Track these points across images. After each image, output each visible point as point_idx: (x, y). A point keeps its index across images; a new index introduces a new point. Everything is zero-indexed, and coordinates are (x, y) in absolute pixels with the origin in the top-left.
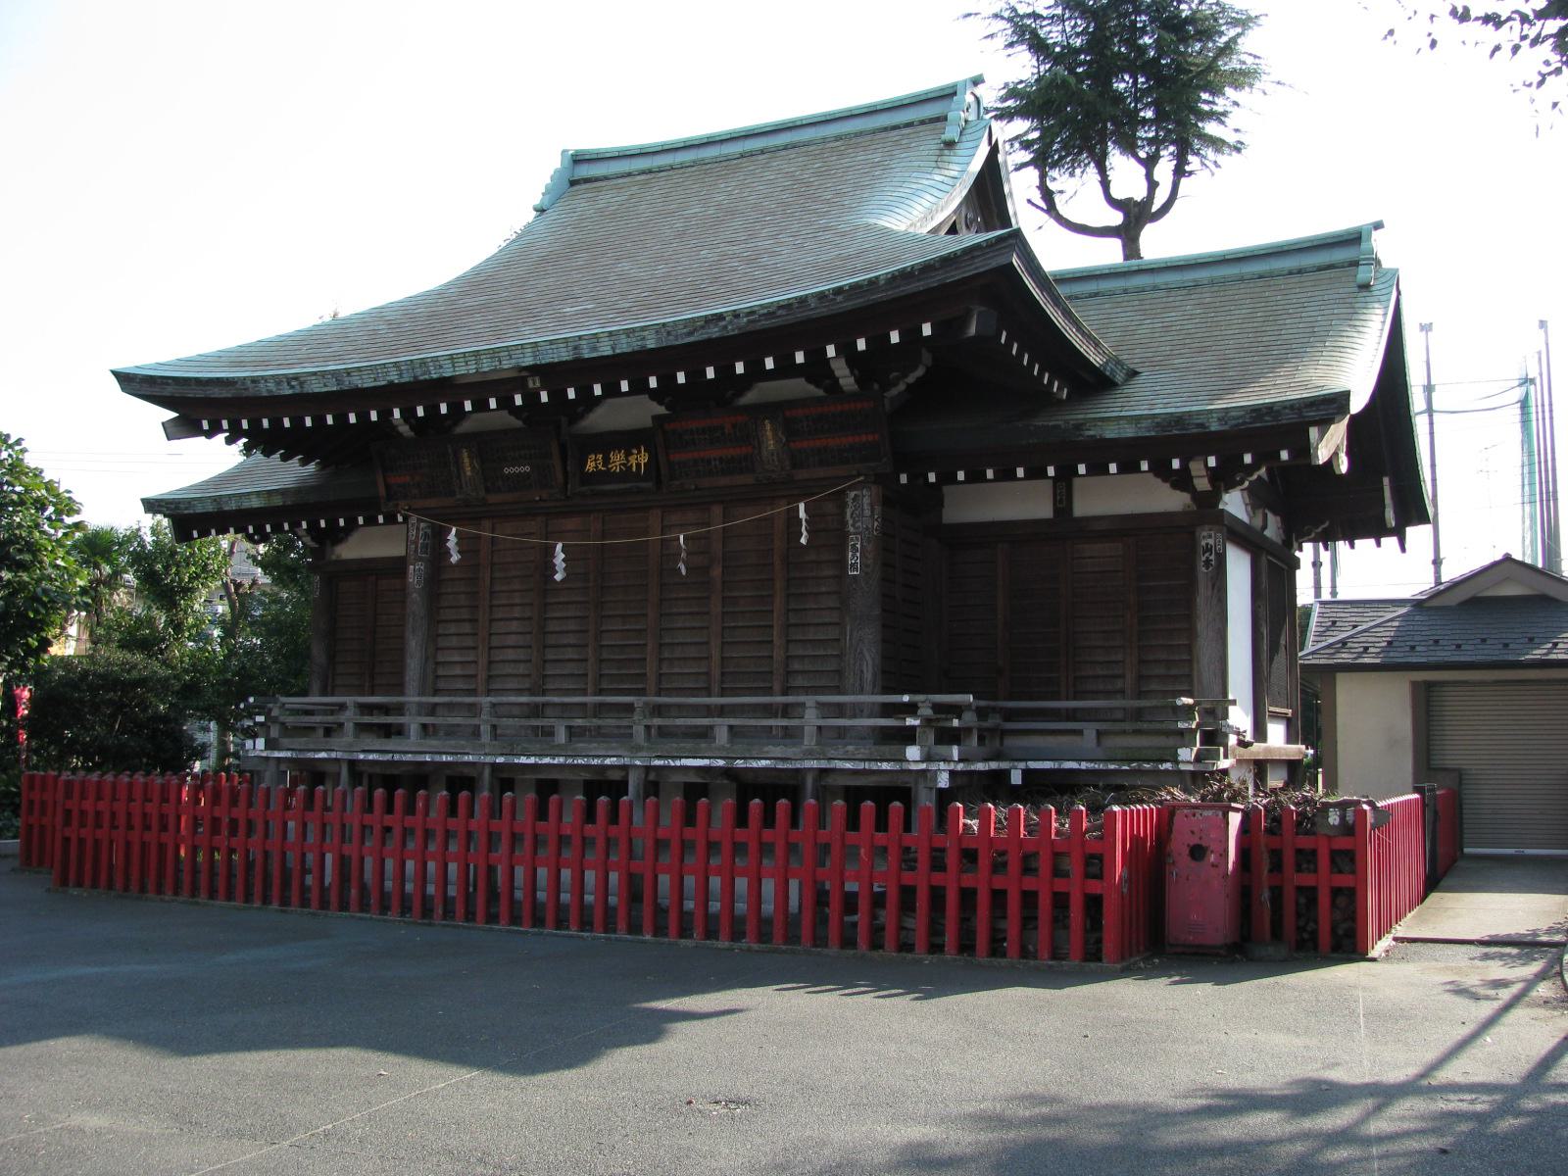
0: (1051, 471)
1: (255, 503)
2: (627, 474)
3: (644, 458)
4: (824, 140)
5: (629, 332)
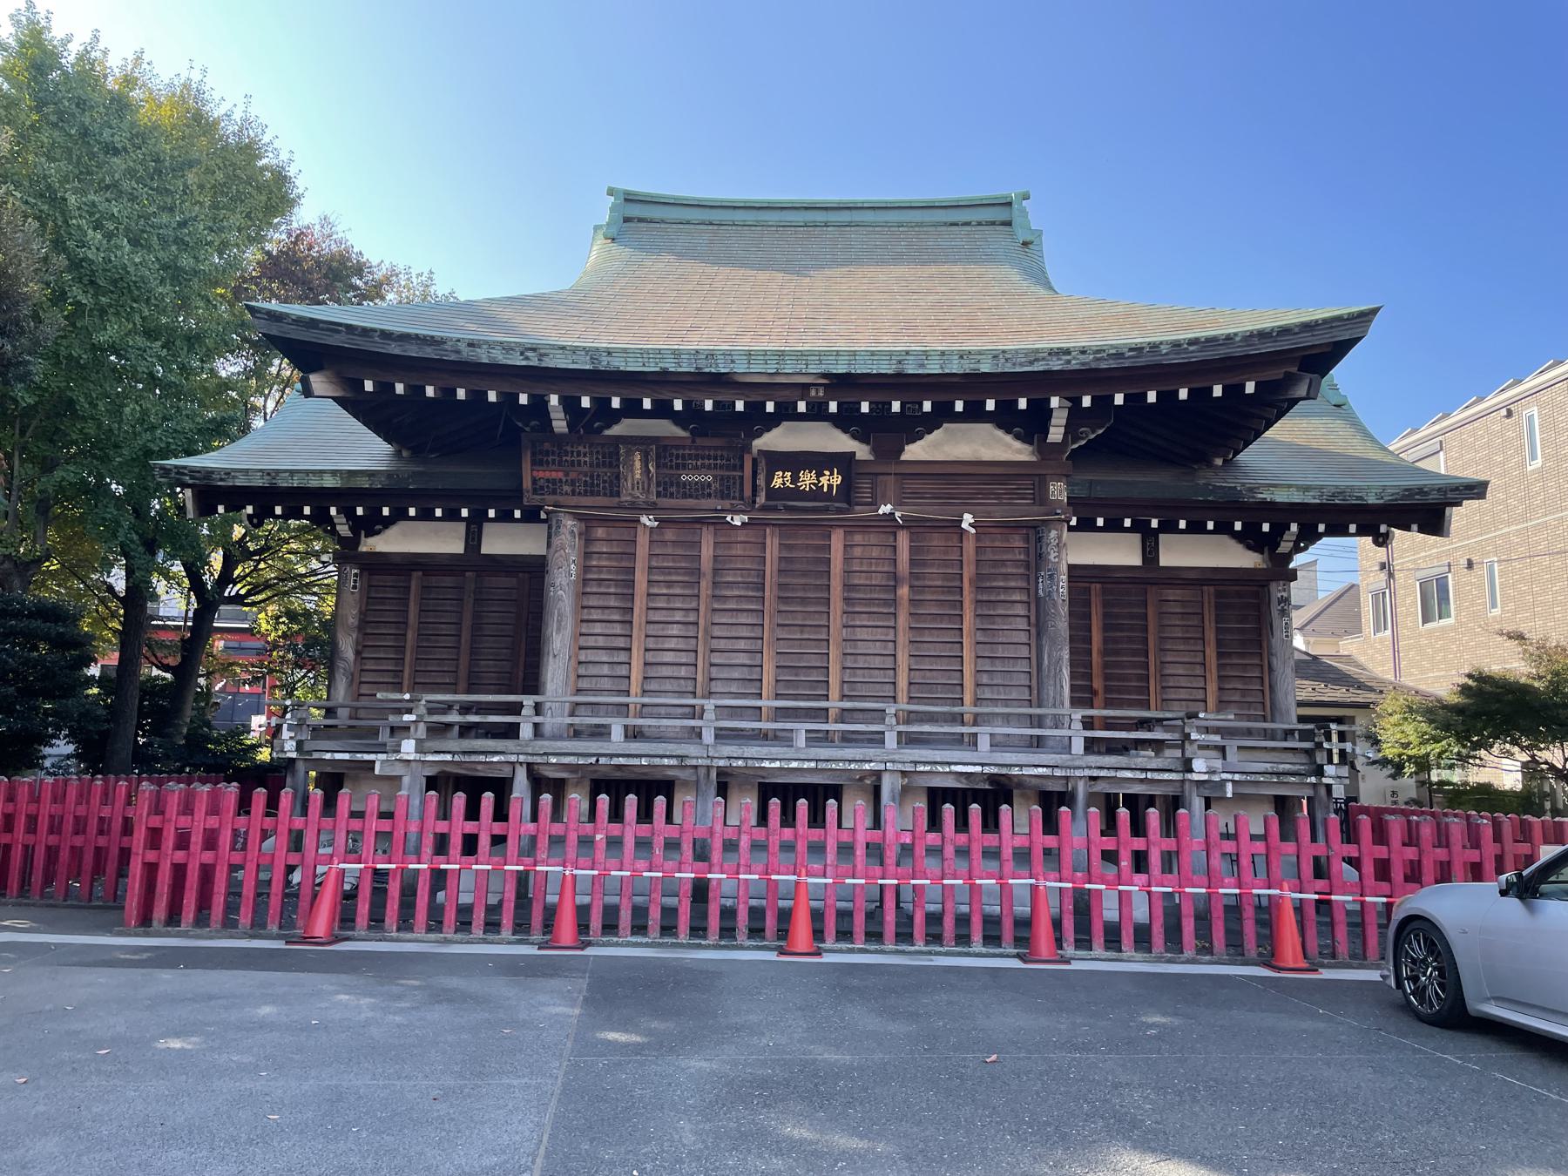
1: (329, 482)
2: (817, 493)
3: (837, 480)
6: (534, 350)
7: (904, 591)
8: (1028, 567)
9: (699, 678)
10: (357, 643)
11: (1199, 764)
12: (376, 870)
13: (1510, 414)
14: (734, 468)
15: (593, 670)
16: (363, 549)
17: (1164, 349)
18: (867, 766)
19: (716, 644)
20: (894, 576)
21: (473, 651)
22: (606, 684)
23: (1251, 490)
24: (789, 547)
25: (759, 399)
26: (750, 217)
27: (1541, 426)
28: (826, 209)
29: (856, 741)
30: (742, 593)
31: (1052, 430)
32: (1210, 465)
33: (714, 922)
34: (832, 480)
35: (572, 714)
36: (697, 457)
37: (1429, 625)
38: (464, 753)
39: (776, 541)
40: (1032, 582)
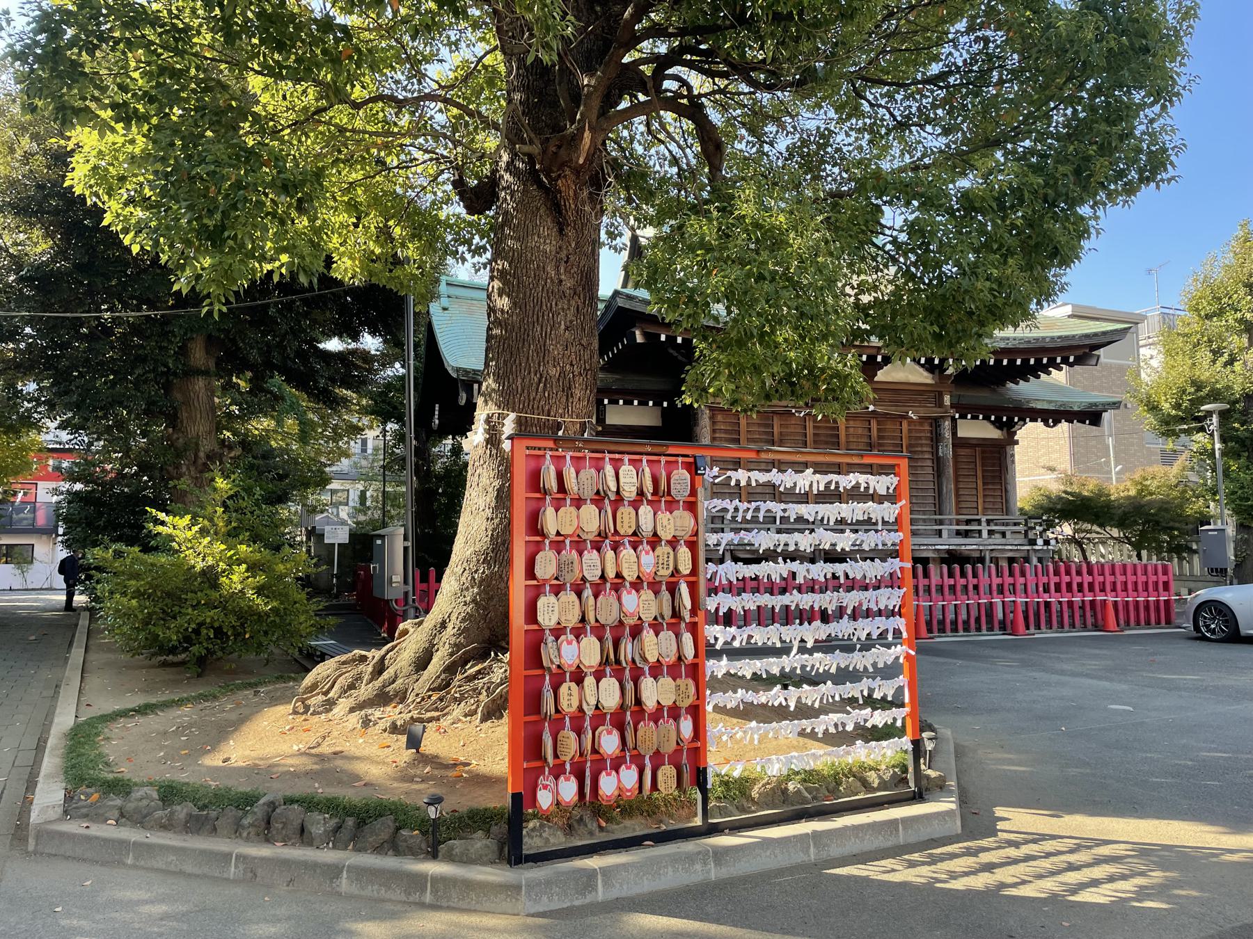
21: (957, 495)
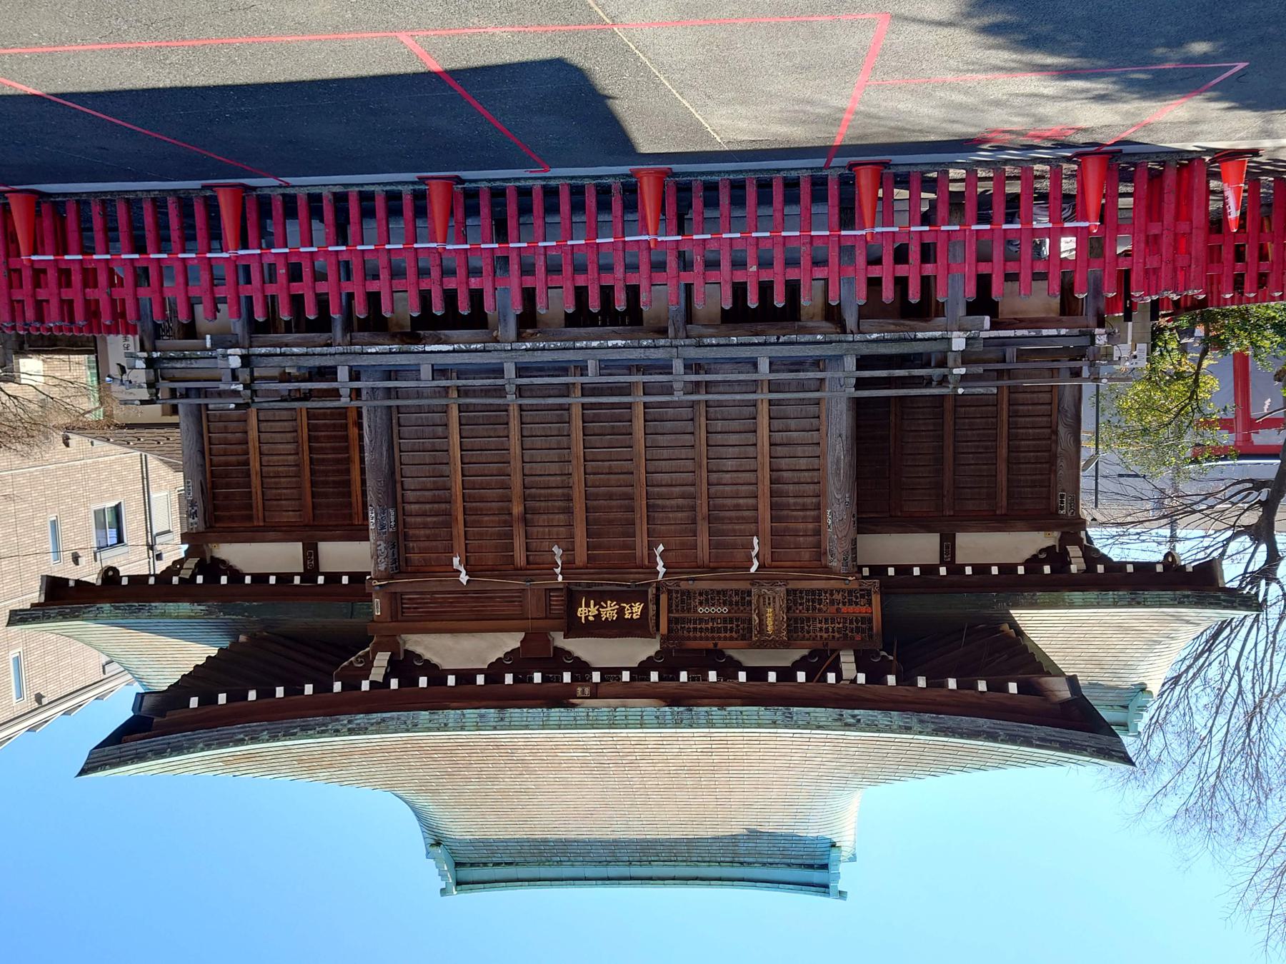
0: (321, 580)
2: (600, 597)
3: (582, 612)
4: (540, 863)
5: (445, 727)
6: (847, 725)
7: (517, 509)
8: (405, 534)
9: (703, 419)
10: (1056, 442)
11: (235, 362)
12: (990, 223)
13: (39, 698)
14: (677, 620)
15: (805, 423)
16: (1056, 534)
17: (265, 735)
18: (529, 345)
19: (690, 453)
20: (526, 522)
22: (790, 410)
23: (210, 613)
24: (625, 546)
25: (637, 683)
26: (704, 871)
27: (9, 688)
28: (631, 878)
29: (555, 369)
30: (668, 502)
31: (385, 664)
32: (252, 637)
33: (833, 189)
34: (586, 612)
35: (822, 380)
36: (713, 630)
37: (113, 504)
38: (905, 340)
39: (638, 553)
40: (401, 522)
